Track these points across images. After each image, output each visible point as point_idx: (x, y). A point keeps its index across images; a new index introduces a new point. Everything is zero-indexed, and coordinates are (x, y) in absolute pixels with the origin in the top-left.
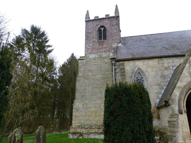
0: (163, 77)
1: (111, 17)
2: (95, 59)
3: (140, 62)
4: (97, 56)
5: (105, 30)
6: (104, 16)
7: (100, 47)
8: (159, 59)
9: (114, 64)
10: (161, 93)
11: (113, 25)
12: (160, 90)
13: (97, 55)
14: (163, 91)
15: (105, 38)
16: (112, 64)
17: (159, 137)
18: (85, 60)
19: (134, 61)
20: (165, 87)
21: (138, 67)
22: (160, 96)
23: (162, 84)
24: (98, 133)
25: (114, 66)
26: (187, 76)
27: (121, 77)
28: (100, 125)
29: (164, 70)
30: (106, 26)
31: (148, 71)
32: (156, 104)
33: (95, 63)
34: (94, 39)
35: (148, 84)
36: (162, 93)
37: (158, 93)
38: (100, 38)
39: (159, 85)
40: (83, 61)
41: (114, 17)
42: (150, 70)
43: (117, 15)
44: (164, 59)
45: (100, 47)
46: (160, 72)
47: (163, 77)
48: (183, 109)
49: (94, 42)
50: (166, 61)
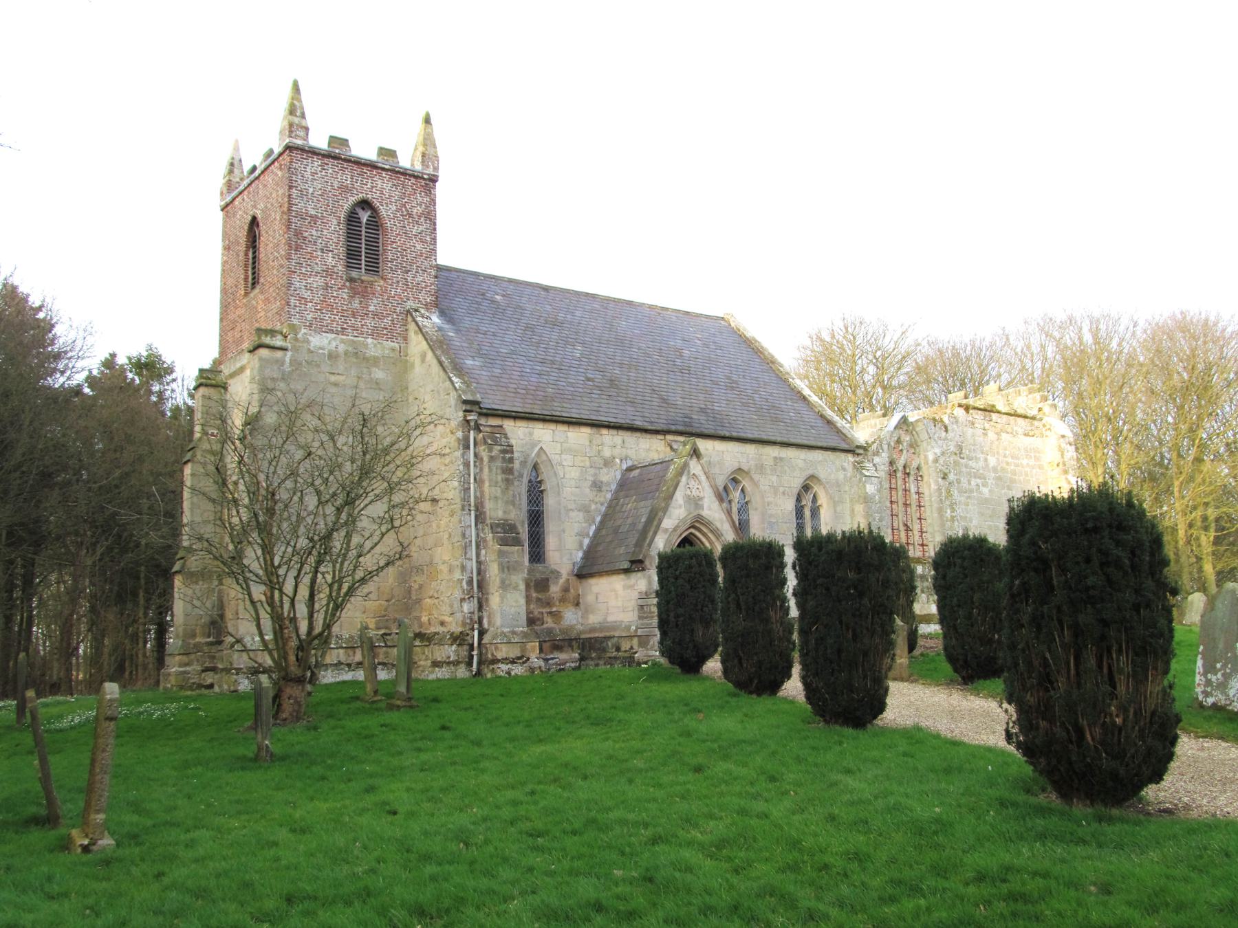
0: (597, 486)
1: (404, 173)
2: (332, 356)
3: (545, 431)
4: (342, 348)
5: (376, 223)
6: (371, 155)
7: (356, 304)
8: (595, 430)
9: (472, 424)
10: (588, 535)
11: (410, 215)
12: (586, 525)
13: (342, 341)
14: (593, 528)
15: (374, 266)
16: (468, 421)
17: (577, 655)
18: (289, 354)
19: (531, 424)
20: (598, 519)
21: (538, 447)
22: (586, 542)
23: (593, 507)
24: (349, 665)
25: (472, 432)
26: (680, 506)
27: (503, 476)
28: (351, 637)
29: (601, 466)
30: (383, 210)
31: (565, 463)
32: (574, 564)
33: (333, 378)
34: (330, 260)
35: (560, 504)
36: (591, 534)
37: (582, 535)
38: (352, 255)
39: (585, 509)
40: (279, 354)
41: (416, 177)
42: (567, 460)
43: (430, 171)
44: (605, 431)
45: (356, 304)
46: (592, 471)
47: (597, 486)
48: (302, 610)
49: (328, 272)
50: (608, 437)
